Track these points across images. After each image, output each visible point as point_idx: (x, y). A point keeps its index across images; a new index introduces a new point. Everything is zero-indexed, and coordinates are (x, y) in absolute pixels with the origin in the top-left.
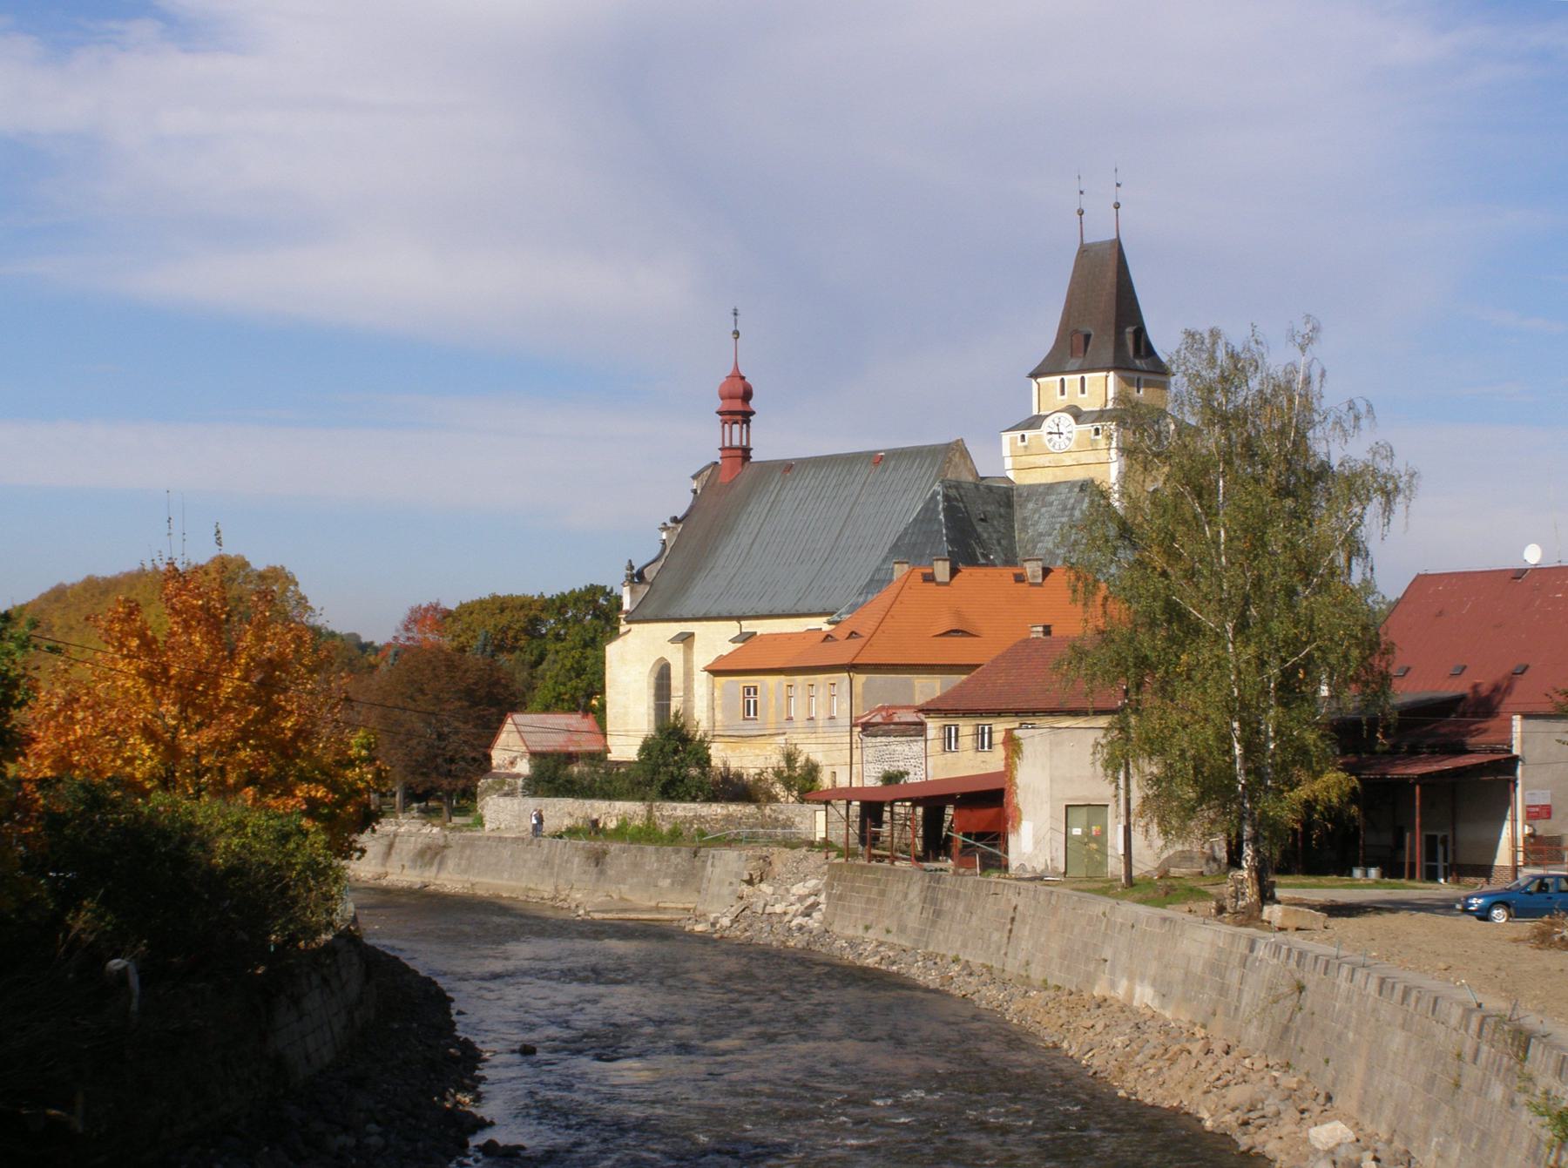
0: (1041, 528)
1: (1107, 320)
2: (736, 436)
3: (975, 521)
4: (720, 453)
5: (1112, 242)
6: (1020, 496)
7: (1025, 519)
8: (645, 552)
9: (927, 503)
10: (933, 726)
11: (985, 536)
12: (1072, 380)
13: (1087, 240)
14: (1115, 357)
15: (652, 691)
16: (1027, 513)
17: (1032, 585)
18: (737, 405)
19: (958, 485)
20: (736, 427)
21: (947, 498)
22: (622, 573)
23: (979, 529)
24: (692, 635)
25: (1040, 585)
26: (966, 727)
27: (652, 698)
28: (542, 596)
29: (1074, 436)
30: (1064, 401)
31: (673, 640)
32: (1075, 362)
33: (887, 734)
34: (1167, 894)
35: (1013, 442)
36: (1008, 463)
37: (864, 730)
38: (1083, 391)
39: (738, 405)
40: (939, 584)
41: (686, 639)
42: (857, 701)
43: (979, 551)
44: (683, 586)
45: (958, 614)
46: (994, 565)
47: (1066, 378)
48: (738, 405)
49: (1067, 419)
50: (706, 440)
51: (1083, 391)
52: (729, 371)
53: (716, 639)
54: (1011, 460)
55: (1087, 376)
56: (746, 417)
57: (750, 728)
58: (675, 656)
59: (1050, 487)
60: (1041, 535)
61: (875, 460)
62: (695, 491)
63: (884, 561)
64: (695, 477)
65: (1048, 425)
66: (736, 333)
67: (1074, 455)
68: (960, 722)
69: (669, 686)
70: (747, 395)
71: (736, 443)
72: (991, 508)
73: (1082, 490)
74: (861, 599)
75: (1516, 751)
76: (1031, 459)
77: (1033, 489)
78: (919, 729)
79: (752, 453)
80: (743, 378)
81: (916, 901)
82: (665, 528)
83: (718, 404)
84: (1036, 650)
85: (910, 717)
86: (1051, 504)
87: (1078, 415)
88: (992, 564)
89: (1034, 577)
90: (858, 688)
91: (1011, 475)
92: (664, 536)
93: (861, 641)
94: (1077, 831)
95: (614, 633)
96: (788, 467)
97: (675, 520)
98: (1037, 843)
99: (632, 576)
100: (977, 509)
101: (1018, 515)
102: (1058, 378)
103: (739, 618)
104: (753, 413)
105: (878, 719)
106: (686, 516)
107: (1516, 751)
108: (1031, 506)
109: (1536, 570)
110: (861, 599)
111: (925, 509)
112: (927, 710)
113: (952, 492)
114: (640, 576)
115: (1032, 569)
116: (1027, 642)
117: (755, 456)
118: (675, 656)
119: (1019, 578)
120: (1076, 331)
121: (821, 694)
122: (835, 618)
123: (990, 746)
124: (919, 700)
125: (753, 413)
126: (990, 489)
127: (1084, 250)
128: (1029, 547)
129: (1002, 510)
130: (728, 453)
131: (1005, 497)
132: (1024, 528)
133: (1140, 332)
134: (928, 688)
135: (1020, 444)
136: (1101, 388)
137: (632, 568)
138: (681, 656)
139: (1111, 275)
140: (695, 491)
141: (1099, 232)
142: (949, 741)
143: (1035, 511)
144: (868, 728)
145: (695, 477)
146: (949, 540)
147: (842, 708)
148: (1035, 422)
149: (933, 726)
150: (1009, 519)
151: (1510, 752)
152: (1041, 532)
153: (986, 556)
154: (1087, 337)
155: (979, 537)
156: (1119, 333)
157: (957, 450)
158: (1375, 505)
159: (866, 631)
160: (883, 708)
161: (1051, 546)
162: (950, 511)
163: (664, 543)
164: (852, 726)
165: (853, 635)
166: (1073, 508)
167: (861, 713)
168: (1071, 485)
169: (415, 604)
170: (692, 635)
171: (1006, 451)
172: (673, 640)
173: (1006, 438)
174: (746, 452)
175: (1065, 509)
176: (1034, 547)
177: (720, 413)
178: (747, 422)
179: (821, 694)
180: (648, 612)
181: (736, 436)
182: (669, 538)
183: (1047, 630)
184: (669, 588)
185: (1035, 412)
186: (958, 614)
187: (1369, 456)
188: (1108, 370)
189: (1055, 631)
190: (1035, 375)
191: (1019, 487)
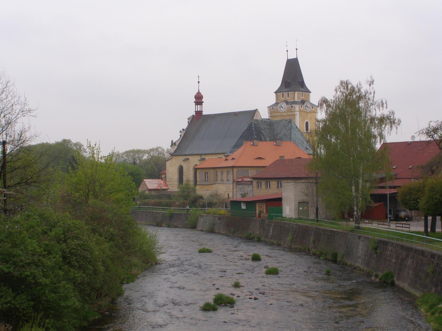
1: (371, 77)
2: (199, 108)
12: (286, 94)
15: (178, 173)
23: (263, 132)
26: (263, 183)
32: (287, 90)
33: (242, 184)
34: (170, 219)
35: (299, 107)
42: (235, 175)
43: (263, 137)
47: (284, 93)
48: (199, 99)
52: (197, 92)
55: (289, 93)
63: (238, 140)
66: (199, 82)
68: (262, 181)
72: (266, 126)
76: (275, 114)
83: (203, 100)
86: (281, 125)
88: (266, 141)
90: (235, 172)
93: (235, 160)
94: (301, 208)
97: (183, 130)
98: (290, 211)
102: (282, 93)
105: (240, 180)
112: (253, 178)
113: (256, 122)
116: (278, 160)
117: (204, 113)
121: (225, 174)
122: (226, 154)
123: (281, 187)
124: (250, 175)
126: (265, 121)
141: (292, 56)
144: (238, 183)
149: (255, 183)
155: (263, 134)
158: (388, 127)
164: (233, 182)
165: (233, 159)
166: (286, 127)
168: (287, 120)
175: (284, 127)
178: (202, 105)
179: (225, 174)
181: (199, 108)
187: (389, 113)
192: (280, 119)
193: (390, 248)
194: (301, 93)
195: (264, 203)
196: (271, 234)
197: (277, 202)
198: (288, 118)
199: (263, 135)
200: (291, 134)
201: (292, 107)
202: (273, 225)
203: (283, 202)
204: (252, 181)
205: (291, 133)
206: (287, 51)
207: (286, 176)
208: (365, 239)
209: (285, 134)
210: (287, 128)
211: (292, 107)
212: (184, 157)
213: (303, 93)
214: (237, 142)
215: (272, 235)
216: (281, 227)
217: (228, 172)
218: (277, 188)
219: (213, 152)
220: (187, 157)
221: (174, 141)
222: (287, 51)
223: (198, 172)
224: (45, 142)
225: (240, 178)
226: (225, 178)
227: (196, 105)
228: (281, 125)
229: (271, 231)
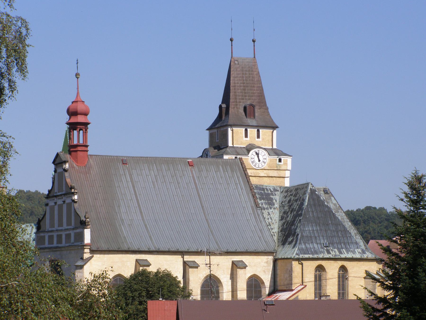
12: (252, 132)
29: (267, 161)
48: (77, 121)
67: (265, 171)
141: (243, 52)
201: (280, 160)
206: (231, 40)
211: (280, 160)
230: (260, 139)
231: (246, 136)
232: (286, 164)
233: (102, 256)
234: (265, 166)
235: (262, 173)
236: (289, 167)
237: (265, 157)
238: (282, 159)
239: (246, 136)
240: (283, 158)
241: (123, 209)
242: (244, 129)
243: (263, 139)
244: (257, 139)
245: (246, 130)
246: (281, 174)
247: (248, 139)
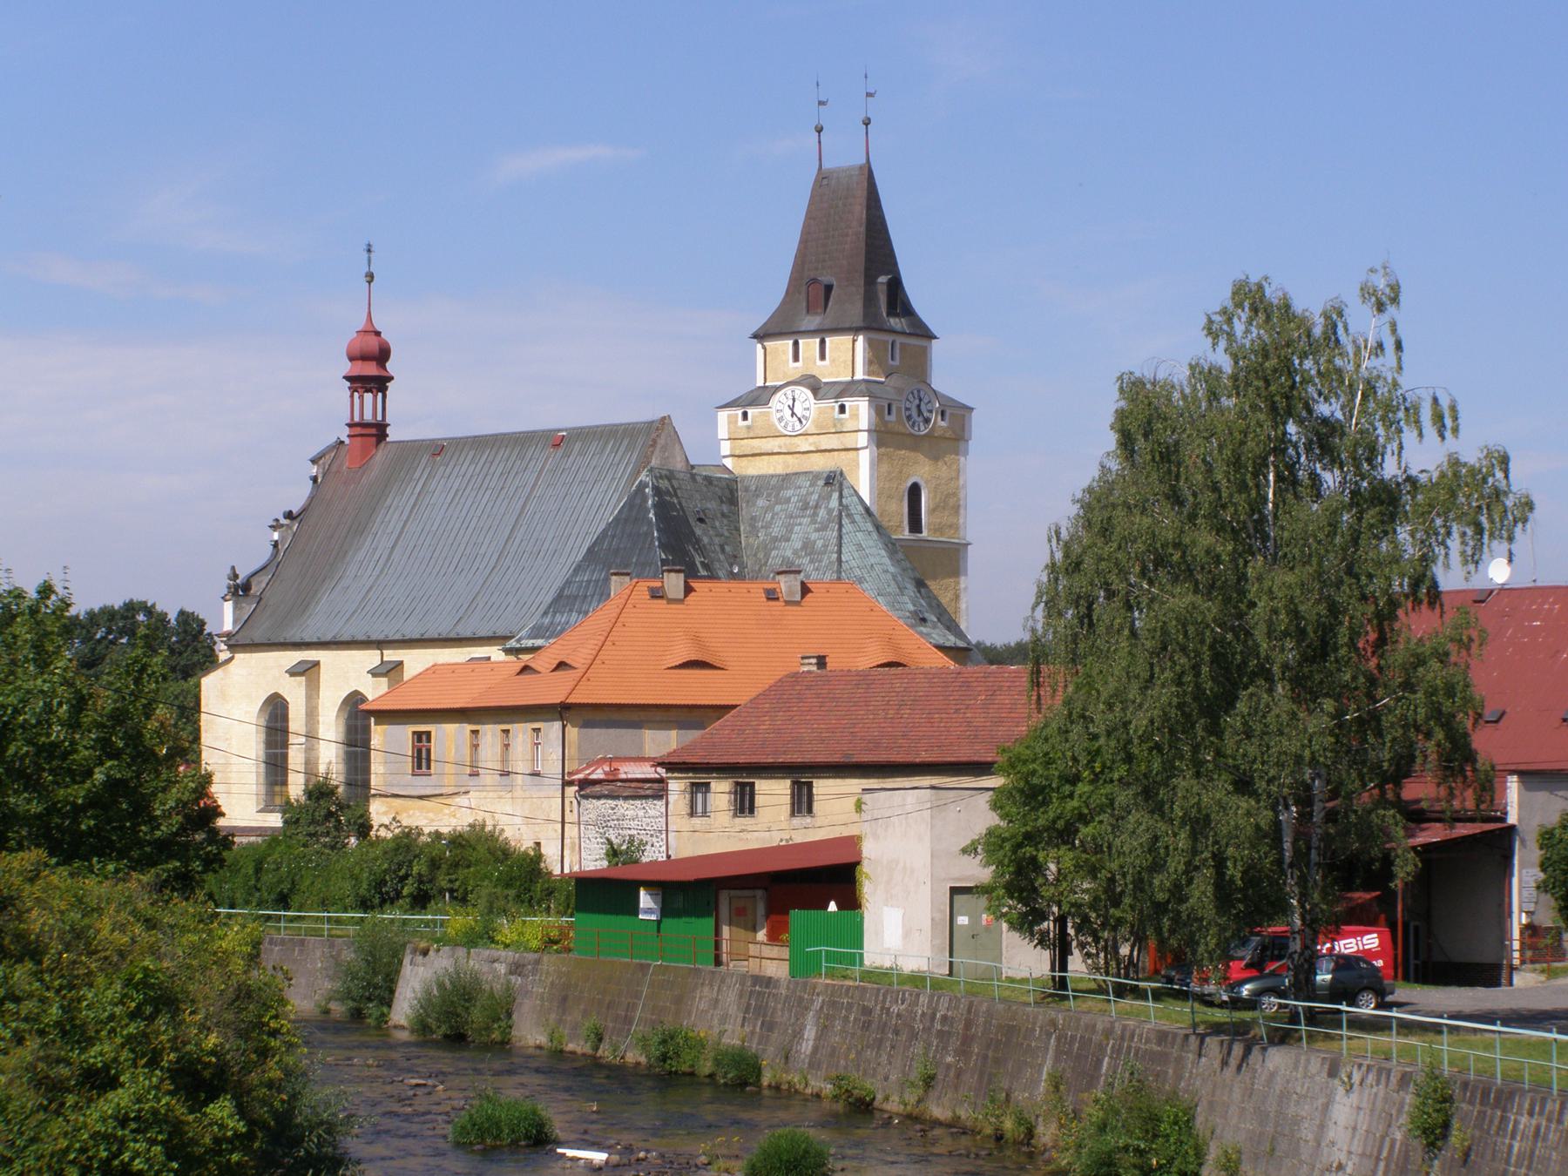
0: (776, 530)
3: (692, 522)
4: (347, 431)
5: (861, 168)
6: (747, 490)
7: (753, 519)
8: (252, 554)
9: (632, 498)
10: (677, 786)
11: (706, 540)
12: (809, 345)
13: (828, 164)
14: (866, 315)
16: (756, 512)
17: (788, 603)
18: (371, 369)
19: (670, 476)
20: (368, 397)
21: (657, 491)
22: (223, 583)
23: (698, 532)
24: (317, 664)
25: (797, 603)
27: (262, 746)
28: (153, 606)
29: (813, 414)
30: (795, 369)
31: (293, 672)
32: (813, 322)
35: (732, 421)
36: (726, 448)
37: (581, 789)
38: (823, 357)
39: (371, 370)
40: (671, 601)
41: (308, 671)
42: (571, 751)
43: (698, 560)
44: (302, 604)
45: (697, 640)
46: (718, 578)
48: (371, 370)
49: (804, 393)
50: (331, 410)
51: (823, 357)
52: (361, 324)
53: (348, 673)
54: (722, 443)
56: (379, 384)
57: (422, 785)
58: (295, 693)
59: (786, 479)
60: (775, 539)
61: (557, 441)
62: (315, 479)
63: (577, 571)
64: (314, 461)
65: (779, 401)
66: (370, 277)
67: (811, 439)
69: (285, 731)
70: (383, 355)
71: (368, 417)
72: (712, 505)
73: (827, 484)
74: (547, 621)
75: (1512, 819)
77: (766, 485)
78: (657, 790)
79: (388, 431)
80: (378, 334)
81: (733, 1010)
82: (276, 526)
84: (809, 688)
85: (646, 771)
86: (788, 500)
87: (816, 387)
89: (791, 593)
91: (728, 463)
92: (276, 536)
95: (209, 662)
96: (438, 449)
97: (289, 515)
98: (907, 934)
99: (236, 587)
100: (693, 505)
101: (745, 512)
103: (380, 644)
104: (391, 378)
105: (598, 774)
106: (304, 510)
107: (1512, 819)
108: (761, 502)
109: (1503, 590)
110: (547, 621)
111: (630, 504)
112: (672, 767)
113: (664, 484)
114: (246, 587)
115: (787, 586)
116: (796, 677)
117: (393, 434)
118: (295, 693)
119: (772, 596)
120: (814, 281)
122: (512, 643)
125: (391, 378)
126: (709, 480)
127: (823, 178)
128: (761, 555)
129: (725, 508)
130: (358, 430)
131: (728, 491)
132: (754, 530)
133: (896, 286)
134: (664, 741)
135: (741, 423)
136: (847, 356)
137: (236, 576)
138: (302, 692)
139: (859, 210)
140: (315, 479)
141: (844, 155)
142: (745, 804)
143: (767, 510)
145: (314, 461)
146: (661, 546)
147: (551, 763)
148: (761, 396)
149: (677, 786)
150: (732, 518)
151: (1503, 819)
152: (783, 534)
153: (706, 566)
154: (829, 288)
155: (698, 541)
156: (870, 281)
157: (658, 432)
159: (579, 659)
160: (604, 760)
161: (789, 553)
162: (662, 507)
163: (276, 545)
165: (562, 665)
166: (817, 506)
167: (575, 766)
168: (815, 476)
169: (109, 603)
170: (317, 664)
171: (723, 432)
172: (293, 672)
173: (723, 416)
174: (377, 431)
175: (805, 507)
176: (767, 556)
177: (347, 378)
178: (383, 390)
180: (257, 635)
182: (283, 538)
183: (822, 662)
184: (277, 603)
185: (760, 383)
186: (697, 640)
188: (856, 330)
189: (831, 664)
190: (761, 336)
191: (744, 478)
192: (780, 470)
193: (1524, 1120)
194: (889, 338)
195: (759, 893)
196: (807, 1046)
197: (830, 881)
198: (820, 464)
199: (701, 550)
200: (840, 546)
201: (842, 409)
202: (817, 1005)
203: (869, 891)
204: (661, 781)
205: (840, 537)
206: (867, 123)
207: (836, 758)
208: (1371, 1078)
209: (808, 546)
210: (822, 513)
211: (842, 409)
212: (294, 657)
213: (900, 340)
214: (568, 583)
215: (816, 1049)
216: (867, 1011)
217: (475, 732)
218: (692, 814)
219: (443, 628)
220: (391, 655)
221: (243, 575)
222: (867, 123)
223: (379, 735)
224: (1064, 512)
225: (604, 760)
226: (520, 765)
227: (353, 390)
228: (788, 500)
229: (810, 1033)
230: (827, 362)
231: (796, 358)
232: (855, 416)
233: (247, 655)
234: (809, 426)
235: (804, 444)
236: (864, 423)
237: (807, 405)
238: (847, 405)
239: (796, 358)
240: (849, 403)
241: (360, 555)
242: (791, 342)
243: (833, 361)
244: (819, 363)
245: (796, 344)
246: (848, 440)
247: (799, 364)
